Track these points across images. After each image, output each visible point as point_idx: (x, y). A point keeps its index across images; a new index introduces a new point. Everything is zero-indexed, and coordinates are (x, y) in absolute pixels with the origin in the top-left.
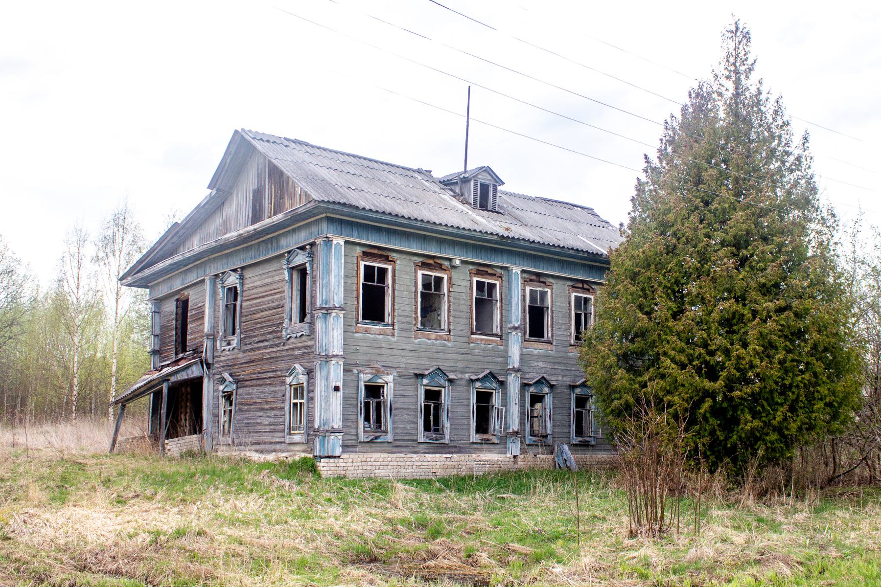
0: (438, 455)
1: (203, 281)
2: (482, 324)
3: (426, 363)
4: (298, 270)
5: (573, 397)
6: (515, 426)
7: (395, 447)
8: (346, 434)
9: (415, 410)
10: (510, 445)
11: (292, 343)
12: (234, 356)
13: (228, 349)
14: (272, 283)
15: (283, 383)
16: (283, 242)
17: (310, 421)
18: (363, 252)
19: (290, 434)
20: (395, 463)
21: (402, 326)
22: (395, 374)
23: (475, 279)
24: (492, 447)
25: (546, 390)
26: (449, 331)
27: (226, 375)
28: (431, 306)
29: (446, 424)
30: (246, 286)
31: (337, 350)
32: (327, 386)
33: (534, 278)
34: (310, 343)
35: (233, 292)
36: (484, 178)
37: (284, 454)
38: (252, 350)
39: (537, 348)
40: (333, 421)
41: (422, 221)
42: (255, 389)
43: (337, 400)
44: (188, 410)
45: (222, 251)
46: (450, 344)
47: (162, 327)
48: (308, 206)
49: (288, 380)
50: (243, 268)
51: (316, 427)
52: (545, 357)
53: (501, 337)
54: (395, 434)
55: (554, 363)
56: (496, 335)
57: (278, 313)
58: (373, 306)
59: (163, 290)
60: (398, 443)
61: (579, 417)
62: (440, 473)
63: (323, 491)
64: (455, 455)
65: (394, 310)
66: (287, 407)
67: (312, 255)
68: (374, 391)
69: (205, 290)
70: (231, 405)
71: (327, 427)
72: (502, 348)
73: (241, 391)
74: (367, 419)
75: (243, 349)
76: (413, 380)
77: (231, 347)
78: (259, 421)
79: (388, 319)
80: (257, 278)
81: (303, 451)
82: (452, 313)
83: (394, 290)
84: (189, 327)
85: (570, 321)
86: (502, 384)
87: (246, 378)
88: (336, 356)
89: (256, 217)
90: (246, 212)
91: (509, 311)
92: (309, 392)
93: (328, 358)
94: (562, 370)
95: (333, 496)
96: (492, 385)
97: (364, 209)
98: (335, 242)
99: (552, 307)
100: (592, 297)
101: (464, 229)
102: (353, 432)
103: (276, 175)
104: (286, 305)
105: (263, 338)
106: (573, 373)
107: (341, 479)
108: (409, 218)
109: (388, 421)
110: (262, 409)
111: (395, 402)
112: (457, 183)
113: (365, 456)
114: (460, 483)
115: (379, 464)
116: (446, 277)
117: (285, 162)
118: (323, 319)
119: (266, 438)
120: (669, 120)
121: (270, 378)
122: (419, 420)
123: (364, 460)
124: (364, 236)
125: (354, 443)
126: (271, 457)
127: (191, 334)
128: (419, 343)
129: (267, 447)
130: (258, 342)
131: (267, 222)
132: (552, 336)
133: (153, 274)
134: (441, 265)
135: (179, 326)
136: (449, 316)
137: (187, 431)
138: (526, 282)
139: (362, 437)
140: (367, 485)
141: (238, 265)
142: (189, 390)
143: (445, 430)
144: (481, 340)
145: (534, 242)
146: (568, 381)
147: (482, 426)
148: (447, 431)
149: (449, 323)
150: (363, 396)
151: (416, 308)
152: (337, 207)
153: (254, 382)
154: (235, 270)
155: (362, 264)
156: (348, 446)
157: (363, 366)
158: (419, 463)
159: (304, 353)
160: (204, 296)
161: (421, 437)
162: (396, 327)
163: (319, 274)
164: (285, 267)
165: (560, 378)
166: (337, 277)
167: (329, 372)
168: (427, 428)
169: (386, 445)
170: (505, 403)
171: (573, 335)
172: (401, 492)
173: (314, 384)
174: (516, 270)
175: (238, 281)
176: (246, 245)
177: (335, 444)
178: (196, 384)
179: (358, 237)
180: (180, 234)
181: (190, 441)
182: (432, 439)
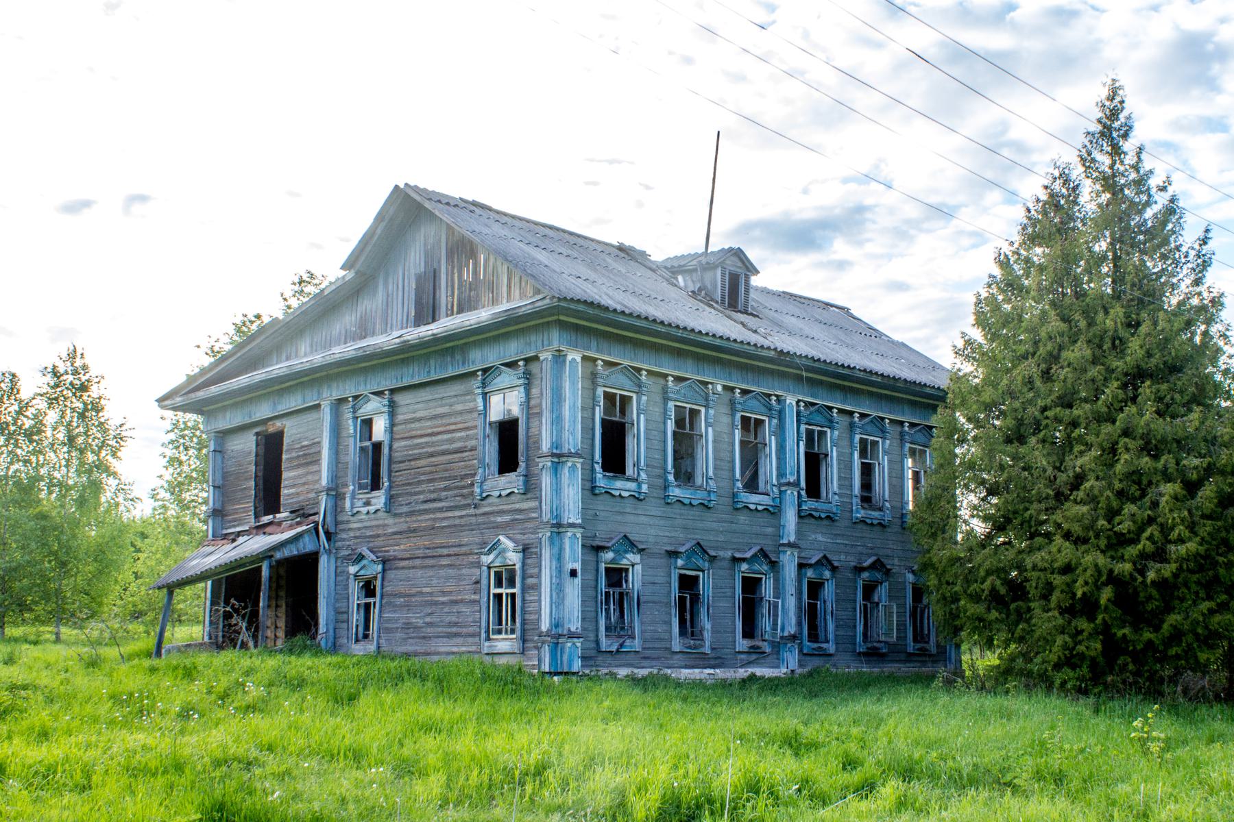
0: (697, 671)
1: (317, 407)
3: (680, 535)
9: (668, 604)
14: (450, 415)
19: (488, 639)
25: (827, 574)
29: (707, 625)
32: (560, 570)
34: (525, 505)
41: (685, 328)
42: (420, 573)
43: (573, 592)
50: (392, 391)
54: (645, 640)
68: (616, 576)
79: (630, 471)
80: (419, 406)
84: (285, 475)
86: (774, 565)
89: (426, 311)
90: (404, 306)
92: (524, 578)
97: (615, 310)
98: (569, 358)
101: (735, 341)
103: (462, 249)
105: (432, 496)
108: (670, 325)
112: (695, 270)
130: (426, 502)
131: (445, 324)
135: (260, 474)
139: (605, 644)
145: (819, 360)
148: (707, 635)
152: (581, 307)
153: (418, 562)
161: (677, 645)
165: (843, 557)
168: (683, 633)
182: (689, 647)
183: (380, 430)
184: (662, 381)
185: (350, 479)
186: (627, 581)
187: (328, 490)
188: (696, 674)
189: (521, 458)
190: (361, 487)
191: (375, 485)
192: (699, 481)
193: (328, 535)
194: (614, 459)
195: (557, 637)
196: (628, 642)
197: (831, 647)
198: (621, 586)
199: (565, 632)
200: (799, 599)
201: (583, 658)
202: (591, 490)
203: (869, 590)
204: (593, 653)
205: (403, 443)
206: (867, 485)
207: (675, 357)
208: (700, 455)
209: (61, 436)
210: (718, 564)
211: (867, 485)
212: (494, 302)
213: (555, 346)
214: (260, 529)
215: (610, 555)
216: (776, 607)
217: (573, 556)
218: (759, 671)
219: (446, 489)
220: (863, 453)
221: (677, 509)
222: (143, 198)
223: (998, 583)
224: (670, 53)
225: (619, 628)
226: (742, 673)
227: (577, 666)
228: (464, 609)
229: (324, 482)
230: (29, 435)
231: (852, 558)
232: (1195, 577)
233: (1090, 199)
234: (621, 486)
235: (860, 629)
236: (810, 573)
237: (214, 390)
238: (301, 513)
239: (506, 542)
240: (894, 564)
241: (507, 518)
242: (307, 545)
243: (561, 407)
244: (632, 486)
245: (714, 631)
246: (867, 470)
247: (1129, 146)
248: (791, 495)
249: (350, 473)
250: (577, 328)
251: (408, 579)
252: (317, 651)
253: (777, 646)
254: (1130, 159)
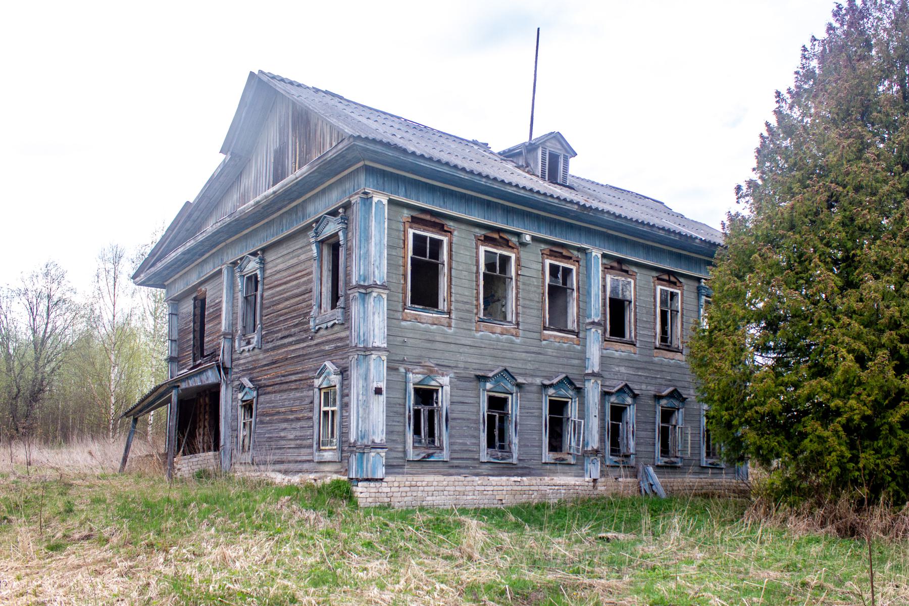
0: (504, 478)
2: (557, 320)
3: (490, 362)
4: (329, 245)
5: (659, 409)
6: (594, 444)
7: (451, 467)
8: (391, 450)
9: (477, 422)
10: (589, 466)
11: (322, 336)
12: (254, 358)
13: (247, 350)
15: (311, 387)
16: (311, 208)
17: (344, 434)
18: (412, 217)
19: (319, 450)
20: (452, 488)
21: (461, 314)
22: (452, 375)
23: (548, 262)
24: (567, 468)
25: (629, 400)
26: (518, 324)
27: (246, 381)
28: (494, 296)
29: (514, 439)
30: (268, 272)
31: (379, 341)
32: (366, 388)
33: (615, 264)
34: (343, 334)
35: (253, 280)
37: (312, 476)
38: (274, 349)
39: (619, 350)
40: (374, 433)
42: (278, 396)
43: (378, 408)
44: (207, 424)
45: (239, 228)
46: (518, 341)
47: (180, 331)
48: (340, 146)
49: (317, 382)
50: (264, 250)
51: (352, 440)
52: (627, 361)
53: (577, 334)
54: (453, 451)
55: (637, 368)
56: (571, 332)
57: (304, 301)
58: (424, 286)
59: (180, 288)
60: (456, 462)
61: (665, 433)
62: (509, 500)
63: (360, 530)
64: (524, 478)
65: (450, 293)
66: (316, 417)
67: (346, 221)
68: (425, 396)
69: (222, 283)
70: (251, 417)
71: (365, 442)
72: (579, 348)
73: (262, 399)
74: (417, 431)
75: (264, 348)
76: (474, 384)
77: (251, 346)
78: (282, 434)
81: (336, 472)
82: (521, 302)
83: (450, 269)
85: (655, 319)
86: (579, 391)
87: (267, 382)
88: (378, 349)
91: (588, 303)
92: (343, 396)
93: (367, 351)
94: (647, 377)
95: (374, 537)
98: (375, 199)
99: (635, 301)
100: (679, 292)
101: (538, 192)
102: (400, 447)
104: (314, 289)
105: (287, 333)
106: (659, 381)
107: (385, 508)
109: (444, 435)
110: (287, 420)
111: (453, 411)
113: (416, 479)
114: (530, 514)
115: (432, 488)
116: (513, 256)
118: (359, 301)
119: (291, 455)
120: (808, 46)
121: (296, 381)
122: (482, 434)
123: (413, 483)
124: (413, 195)
125: (400, 462)
126: (296, 479)
127: (209, 335)
128: (482, 338)
129: (292, 466)
130: (282, 338)
131: (290, 178)
132: (636, 336)
133: (166, 268)
134: (508, 241)
136: (517, 305)
137: (200, 446)
138: (607, 269)
139: (411, 455)
140: (420, 518)
142: (207, 399)
143: (513, 447)
144: (555, 337)
146: (652, 390)
147: (556, 444)
148: (515, 449)
149: (517, 314)
150: (412, 402)
151: (478, 293)
153: (277, 388)
154: (254, 254)
155: (411, 232)
156: (393, 466)
157: (412, 363)
158: (482, 488)
159: (336, 348)
160: (222, 289)
161: (484, 455)
162: (453, 316)
163: (355, 243)
164: (313, 240)
165: (644, 387)
166: (378, 248)
167: (368, 370)
168: (491, 444)
169: (441, 464)
170: (582, 414)
171: (658, 336)
172: (475, 532)
173: (349, 387)
174: (596, 253)
175: (258, 266)
176: (266, 221)
177: (376, 462)
178: (213, 392)
179: (406, 196)
180: (194, 217)
181: (205, 459)
186: (437, 403)
198: (432, 405)
199: (370, 443)
200: (602, 419)
203: (667, 415)
205: (270, 292)
207: (495, 221)
216: (580, 426)
231: (653, 388)
240: (691, 394)
243: (368, 244)
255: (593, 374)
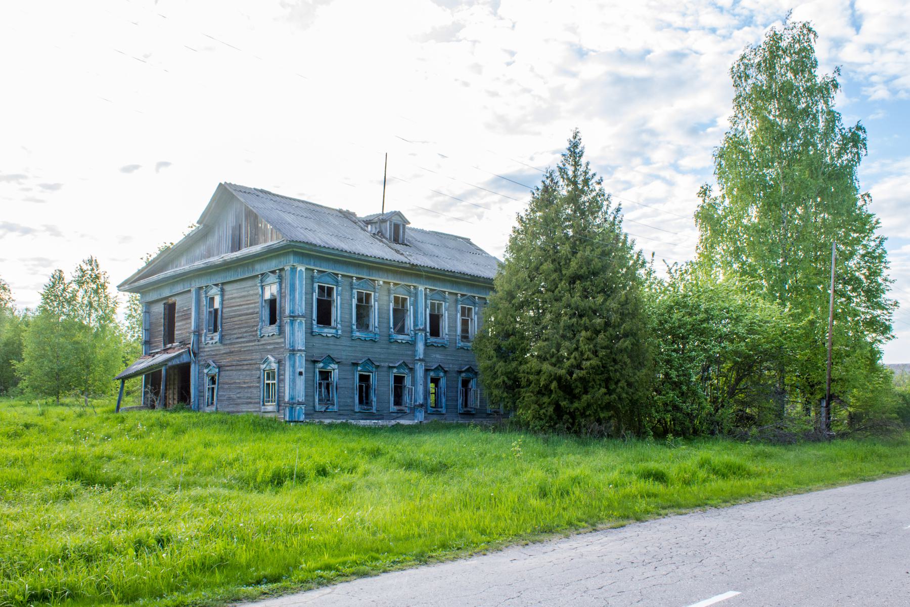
1: (190, 291)
9: (353, 389)
14: (248, 296)
19: (264, 405)
25: (442, 374)
32: (294, 372)
34: (279, 341)
36: (396, 219)
43: (301, 382)
50: (223, 284)
68: (325, 375)
79: (333, 324)
84: (176, 324)
86: (412, 370)
89: (236, 245)
90: (227, 243)
92: (279, 376)
96: (404, 372)
98: (299, 269)
103: (252, 217)
117: (256, 205)
131: (245, 251)
139: (318, 407)
141: (220, 280)
147: (398, 401)
152: (302, 245)
153: (234, 368)
168: (361, 402)
170: (414, 383)
183: (217, 305)
184: (350, 280)
185: (204, 326)
187: (194, 332)
188: (368, 422)
189: (278, 318)
190: (209, 331)
191: (215, 331)
192: (371, 328)
193: (194, 353)
194: (324, 317)
195: (292, 404)
196: (331, 407)
197: (443, 410)
201: (306, 414)
202: (310, 333)
203: (465, 383)
204: (312, 412)
206: (465, 330)
208: (372, 316)
209: (86, 302)
210: (380, 369)
211: (465, 330)
212: (265, 241)
213: (291, 263)
214: (166, 350)
215: (321, 365)
217: (301, 364)
218: (402, 422)
219: (246, 332)
220: (463, 314)
221: (358, 342)
222: (166, 164)
223: (506, 379)
224: (456, 80)
225: (327, 400)
226: (393, 422)
227: (302, 418)
228: (255, 391)
229: (193, 328)
230: (69, 302)
232: (598, 377)
233: (564, 190)
234: (327, 331)
235: (460, 401)
236: (432, 374)
237: (142, 282)
238: (183, 343)
239: (272, 359)
241: (272, 347)
242: (185, 359)
244: (334, 331)
245: (378, 402)
246: (465, 323)
247: (583, 161)
248: (421, 335)
249: (204, 323)
250: (303, 255)
251: (230, 376)
252: (189, 410)
253: (413, 410)
254: (582, 169)
255: (420, 360)
